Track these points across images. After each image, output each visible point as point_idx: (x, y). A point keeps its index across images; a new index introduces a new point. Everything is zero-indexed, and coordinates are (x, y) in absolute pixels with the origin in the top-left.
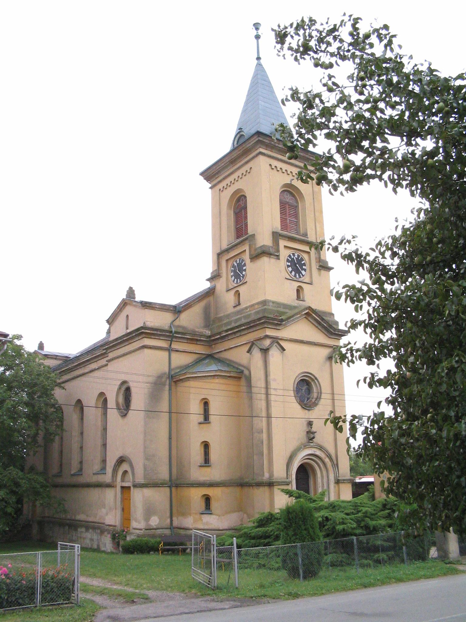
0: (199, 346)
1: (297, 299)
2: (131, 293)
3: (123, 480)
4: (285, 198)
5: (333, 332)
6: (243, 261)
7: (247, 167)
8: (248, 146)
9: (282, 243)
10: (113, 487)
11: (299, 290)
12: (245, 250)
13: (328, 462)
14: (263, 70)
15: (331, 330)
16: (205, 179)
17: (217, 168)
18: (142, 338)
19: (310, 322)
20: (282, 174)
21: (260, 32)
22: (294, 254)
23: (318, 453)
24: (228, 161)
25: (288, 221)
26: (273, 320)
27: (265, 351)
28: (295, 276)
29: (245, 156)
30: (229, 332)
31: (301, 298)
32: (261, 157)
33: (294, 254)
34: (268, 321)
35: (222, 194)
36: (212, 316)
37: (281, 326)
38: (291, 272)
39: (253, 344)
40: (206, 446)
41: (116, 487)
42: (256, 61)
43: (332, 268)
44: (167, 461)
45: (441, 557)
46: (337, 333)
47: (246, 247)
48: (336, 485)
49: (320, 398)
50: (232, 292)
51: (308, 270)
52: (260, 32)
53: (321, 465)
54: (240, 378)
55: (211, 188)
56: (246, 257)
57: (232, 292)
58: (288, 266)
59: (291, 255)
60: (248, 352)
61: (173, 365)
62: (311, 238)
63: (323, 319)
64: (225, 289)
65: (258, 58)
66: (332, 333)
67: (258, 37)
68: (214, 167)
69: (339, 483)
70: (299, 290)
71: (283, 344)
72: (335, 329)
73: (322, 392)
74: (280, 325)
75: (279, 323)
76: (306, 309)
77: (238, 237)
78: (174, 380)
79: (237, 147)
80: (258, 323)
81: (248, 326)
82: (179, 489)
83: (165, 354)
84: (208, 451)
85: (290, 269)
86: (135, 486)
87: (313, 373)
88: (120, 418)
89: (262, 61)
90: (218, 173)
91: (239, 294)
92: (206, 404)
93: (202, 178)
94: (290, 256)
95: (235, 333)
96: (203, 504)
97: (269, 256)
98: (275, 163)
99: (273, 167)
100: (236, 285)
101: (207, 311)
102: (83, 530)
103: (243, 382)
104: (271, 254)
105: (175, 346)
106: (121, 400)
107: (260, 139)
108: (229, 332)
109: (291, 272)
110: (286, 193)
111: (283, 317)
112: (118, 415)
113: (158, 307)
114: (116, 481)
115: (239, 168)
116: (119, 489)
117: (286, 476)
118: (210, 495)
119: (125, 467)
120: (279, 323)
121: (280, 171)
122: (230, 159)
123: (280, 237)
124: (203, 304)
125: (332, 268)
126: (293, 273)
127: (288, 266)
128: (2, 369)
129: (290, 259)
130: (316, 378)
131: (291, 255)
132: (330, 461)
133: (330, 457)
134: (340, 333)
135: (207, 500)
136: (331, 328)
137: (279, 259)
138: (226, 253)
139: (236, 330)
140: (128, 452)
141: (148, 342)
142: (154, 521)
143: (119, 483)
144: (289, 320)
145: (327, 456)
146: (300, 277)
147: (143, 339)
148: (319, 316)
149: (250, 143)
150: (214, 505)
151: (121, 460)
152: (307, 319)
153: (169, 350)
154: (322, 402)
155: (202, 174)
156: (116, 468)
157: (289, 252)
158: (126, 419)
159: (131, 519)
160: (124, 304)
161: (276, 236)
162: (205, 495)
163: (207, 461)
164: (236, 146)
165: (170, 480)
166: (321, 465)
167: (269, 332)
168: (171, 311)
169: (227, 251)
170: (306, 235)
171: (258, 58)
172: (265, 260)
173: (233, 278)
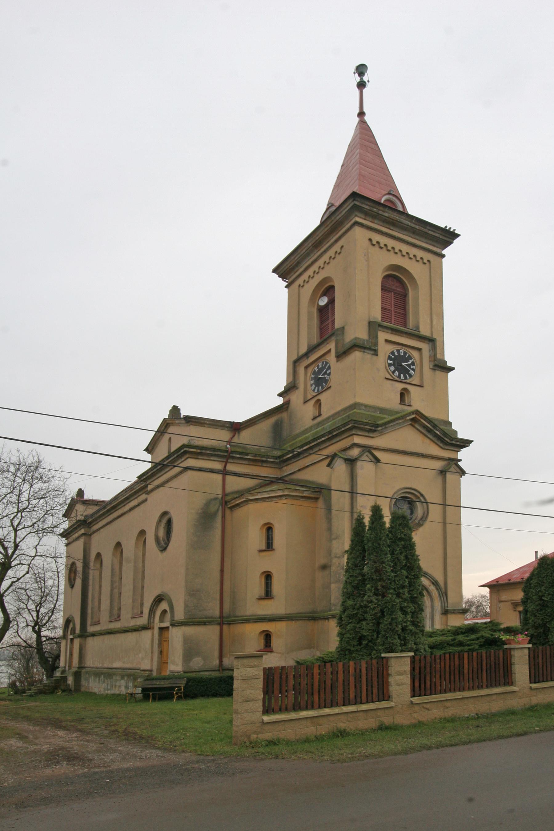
0: (265, 468)
1: (400, 404)
2: (175, 410)
3: (161, 620)
5: (448, 441)
6: (327, 363)
7: (337, 247)
8: (338, 218)
9: (382, 336)
10: (150, 628)
12: (330, 351)
15: (446, 439)
16: (279, 277)
17: (296, 258)
18: (185, 460)
19: (418, 429)
20: (387, 252)
21: (365, 79)
24: (310, 244)
26: (363, 425)
27: (351, 462)
28: (399, 376)
29: (335, 233)
30: (305, 448)
31: (406, 402)
32: (357, 229)
33: (398, 351)
34: (356, 425)
35: (302, 290)
36: (285, 434)
37: (375, 433)
38: (394, 372)
39: (333, 457)
40: (268, 576)
41: (153, 628)
43: (452, 369)
44: (218, 596)
46: (454, 442)
47: (331, 346)
48: (444, 617)
50: (312, 402)
51: (417, 370)
52: (365, 79)
54: (317, 499)
55: (286, 287)
56: (332, 358)
57: (312, 402)
58: (390, 365)
60: (328, 465)
61: (229, 489)
62: (424, 331)
64: (302, 401)
65: (361, 114)
66: (446, 444)
67: (361, 85)
68: (292, 258)
69: (448, 613)
70: (403, 394)
71: (378, 454)
72: (452, 439)
74: (374, 431)
75: (373, 428)
76: (413, 413)
77: (321, 338)
78: (229, 506)
80: (343, 429)
81: (330, 436)
82: (232, 626)
83: (219, 477)
84: (271, 582)
85: (392, 368)
86: (173, 625)
87: (417, 489)
88: (159, 553)
89: (366, 118)
91: (320, 404)
92: (269, 529)
93: (276, 276)
94: (393, 353)
95: (311, 448)
96: (262, 641)
97: (363, 350)
98: (376, 237)
99: (374, 242)
101: (277, 429)
102: (118, 678)
103: (321, 503)
105: (231, 467)
106: (162, 533)
107: (356, 203)
108: (305, 448)
109: (394, 372)
110: (390, 279)
111: (379, 422)
112: (158, 550)
113: (207, 422)
114: (153, 622)
115: (325, 251)
116: (156, 631)
118: (271, 630)
119: (164, 606)
120: (373, 428)
121: (385, 248)
122: (314, 241)
123: (380, 329)
124: (271, 421)
125: (452, 369)
126: (397, 373)
127: (390, 365)
129: (393, 357)
130: (422, 495)
131: (395, 351)
132: (437, 589)
134: (458, 443)
135: (267, 637)
137: (377, 355)
138: (305, 358)
139: (313, 444)
140: (166, 589)
141: (191, 462)
142: (197, 663)
143: (157, 624)
144: (387, 426)
145: (433, 583)
146: (406, 378)
147: (187, 460)
149: (342, 212)
150: (275, 643)
151: (159, 600)
152: (413, 426)
153: (224, 473)
154: (427, 525)
155: (275, 271)
156: (153, 608)
158: (165, 553)
159: (169, 661)
160: (165, 425)
161: (373, 327)
162: (263, 632)
163: (268, 594)
165: (221, 617)
167: (357, 440)
168: (226, 429)
169: (306, 355)
170: (417, 328)
171: (361, 114)
172: (357, 355)
173: (314, 386)
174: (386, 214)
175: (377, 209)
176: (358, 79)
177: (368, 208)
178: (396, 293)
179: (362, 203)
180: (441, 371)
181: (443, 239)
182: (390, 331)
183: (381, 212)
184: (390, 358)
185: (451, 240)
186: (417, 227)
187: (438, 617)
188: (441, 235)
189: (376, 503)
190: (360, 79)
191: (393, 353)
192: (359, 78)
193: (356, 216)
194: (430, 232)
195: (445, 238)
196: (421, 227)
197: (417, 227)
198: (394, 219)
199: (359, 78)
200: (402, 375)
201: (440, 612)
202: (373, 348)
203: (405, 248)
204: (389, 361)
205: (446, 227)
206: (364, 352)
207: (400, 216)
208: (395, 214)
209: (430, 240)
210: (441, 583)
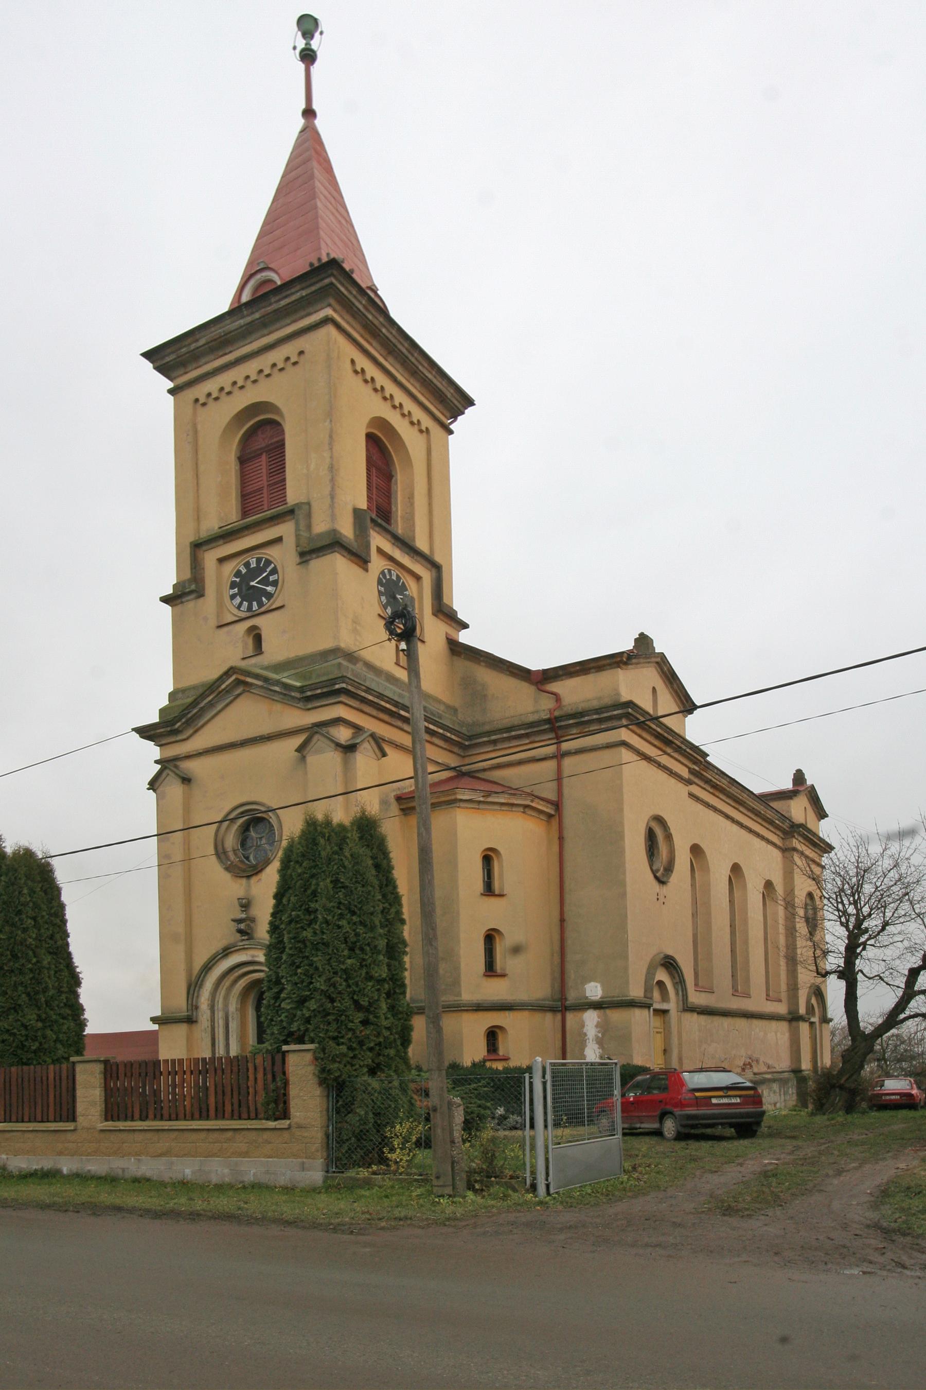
32: (331, 329)
45: (711, 1197)
55: (171, 392)
59: (386, 571)
65: (309, 113)
77: (245, 513)
79: (247, 304)
89: (318, 123)
90: (195, 357)
94: (383, 573)
100: (243, 615)
105: (565, 746)
128: (2, 914)
129: (384, 581)
131: (386, 571)
164: (245, 298)
171: (309, 113)
174: (202, 342)
175: (185, 346)
176: (301, 44)
178: (270, 450)
179: (163, 358)
180: (318, 557)
181: (311, 293)
182: (221, 542)
183: (193, 346)
188: (303, 289)
189: (364, 814)
190: (306, 44)
192: (304, 42)
193: (330, 305)
194: (283, 303)
195: (313, 288)
196: (263, 310)
197: (257, 315)
198: (215, 337)
199: (304, 42)
202: (187, 590)
205: (311, 265)
206: (182, 603)
207: (221, 325)
208: (213, 329)
209: (296, 311)
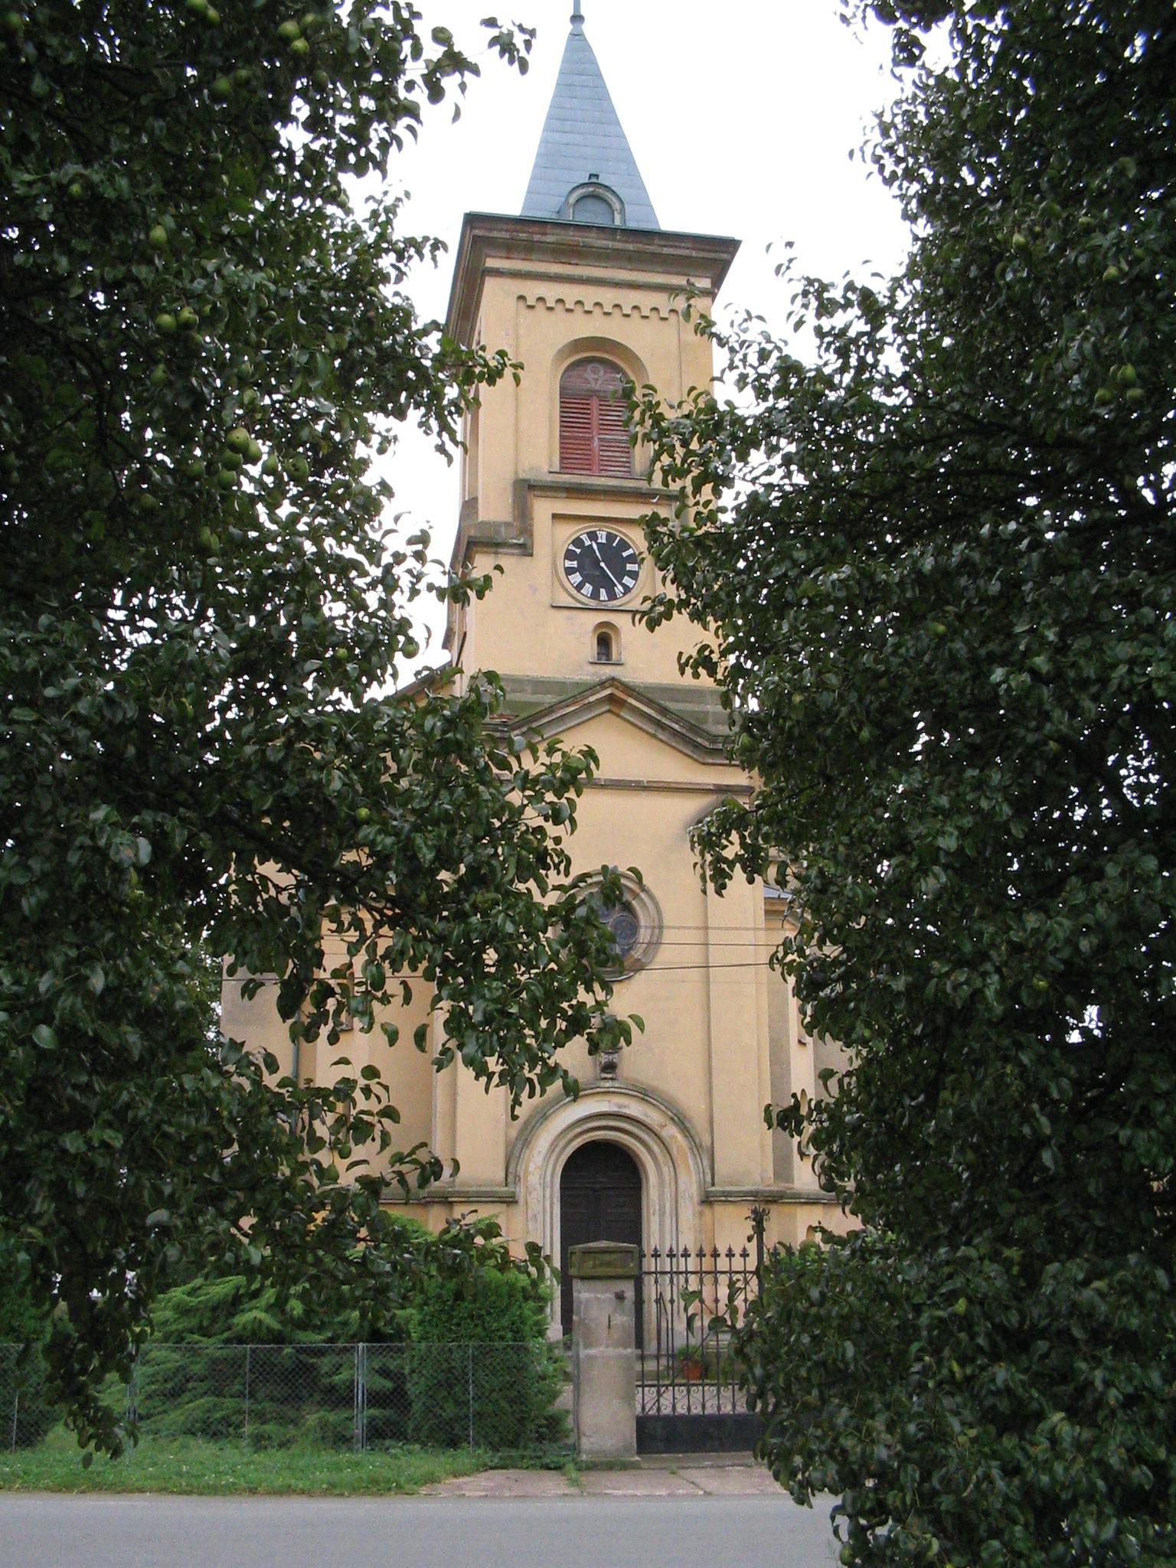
4: (587, 381)
9: (543, 509)
11: (604, 641)
13: (673, 1137)
14: (587, 48)
22: (593, 536)
23: (635, 1109)
25: (596, 443)
28: (595, 595)
33: (593, 536)
38: (579, 587)
42: (569, 27)
49: (659, 943)
53: (656, 1148)
59: (584, 537)
63: (664, 711)
70: (604, 641)
73: (666, 923)
94: (578, 542)
98: (534, 290)
104: (498, 545)
107: (477, 232)
110: (589, 367)
117: (502, 1174)
126: (588, 588)
127: (569, 571)
131: (584, 537)
133: (681, 1121)
136: (697, 734)
148: (649, 702)
157: (567, 533)
166: (656, 1148)
171: (577, 18)
177: (507, 235)
183: (536, 238)
184: (569, 555)
185: (725, 256)
186: (631, 247)
187: (689, 1210)
191: (578, 542)
194: (666, 251)
195: (706, 255)
197: (631, 247)
200: (603, 591)
201: (696, 1199)
203: (608, 296)
204: (568, 564)
210: (699, 1123)
